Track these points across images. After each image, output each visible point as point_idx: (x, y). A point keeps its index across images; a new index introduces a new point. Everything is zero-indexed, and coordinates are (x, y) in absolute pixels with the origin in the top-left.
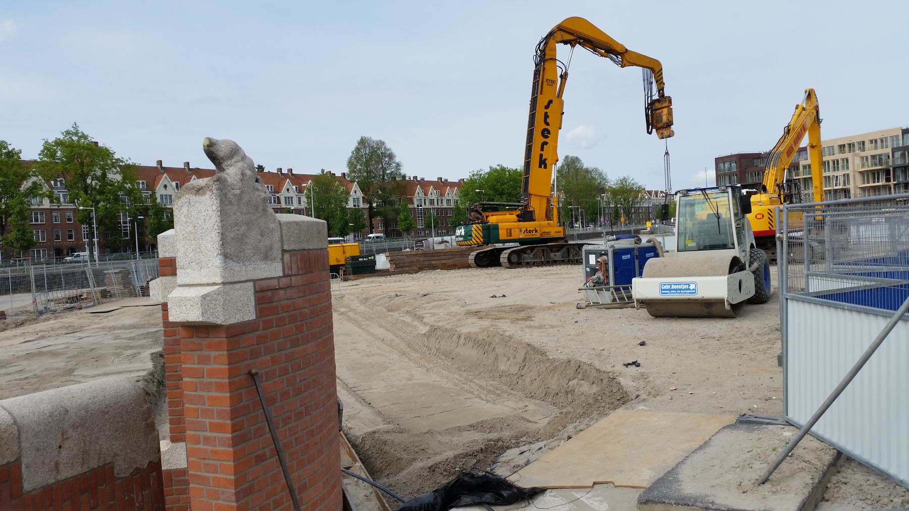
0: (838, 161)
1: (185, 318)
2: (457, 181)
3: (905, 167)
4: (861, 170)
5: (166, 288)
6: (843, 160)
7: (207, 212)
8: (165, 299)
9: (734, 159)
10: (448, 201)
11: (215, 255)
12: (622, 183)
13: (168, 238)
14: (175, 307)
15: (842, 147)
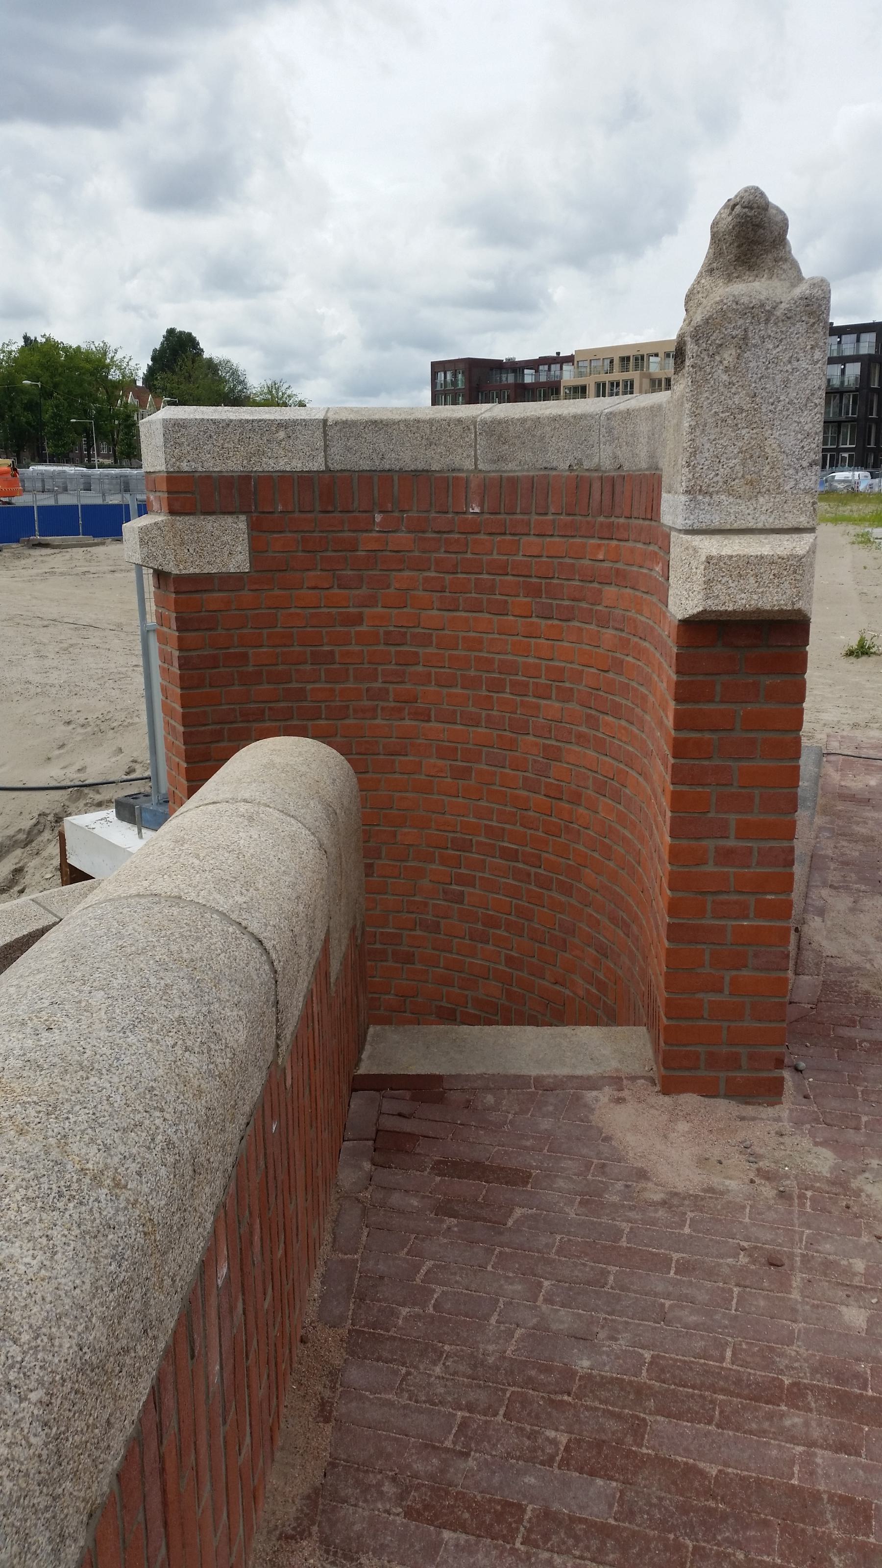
0: (604, 385)
1: (753, 602)
5: (182, 543)
7: (795, 364)
8: (181, 567)
11: (805, 464)
12: (270, 392)
13: (185, 427)
14: (725, 579)
15: (625, 360)
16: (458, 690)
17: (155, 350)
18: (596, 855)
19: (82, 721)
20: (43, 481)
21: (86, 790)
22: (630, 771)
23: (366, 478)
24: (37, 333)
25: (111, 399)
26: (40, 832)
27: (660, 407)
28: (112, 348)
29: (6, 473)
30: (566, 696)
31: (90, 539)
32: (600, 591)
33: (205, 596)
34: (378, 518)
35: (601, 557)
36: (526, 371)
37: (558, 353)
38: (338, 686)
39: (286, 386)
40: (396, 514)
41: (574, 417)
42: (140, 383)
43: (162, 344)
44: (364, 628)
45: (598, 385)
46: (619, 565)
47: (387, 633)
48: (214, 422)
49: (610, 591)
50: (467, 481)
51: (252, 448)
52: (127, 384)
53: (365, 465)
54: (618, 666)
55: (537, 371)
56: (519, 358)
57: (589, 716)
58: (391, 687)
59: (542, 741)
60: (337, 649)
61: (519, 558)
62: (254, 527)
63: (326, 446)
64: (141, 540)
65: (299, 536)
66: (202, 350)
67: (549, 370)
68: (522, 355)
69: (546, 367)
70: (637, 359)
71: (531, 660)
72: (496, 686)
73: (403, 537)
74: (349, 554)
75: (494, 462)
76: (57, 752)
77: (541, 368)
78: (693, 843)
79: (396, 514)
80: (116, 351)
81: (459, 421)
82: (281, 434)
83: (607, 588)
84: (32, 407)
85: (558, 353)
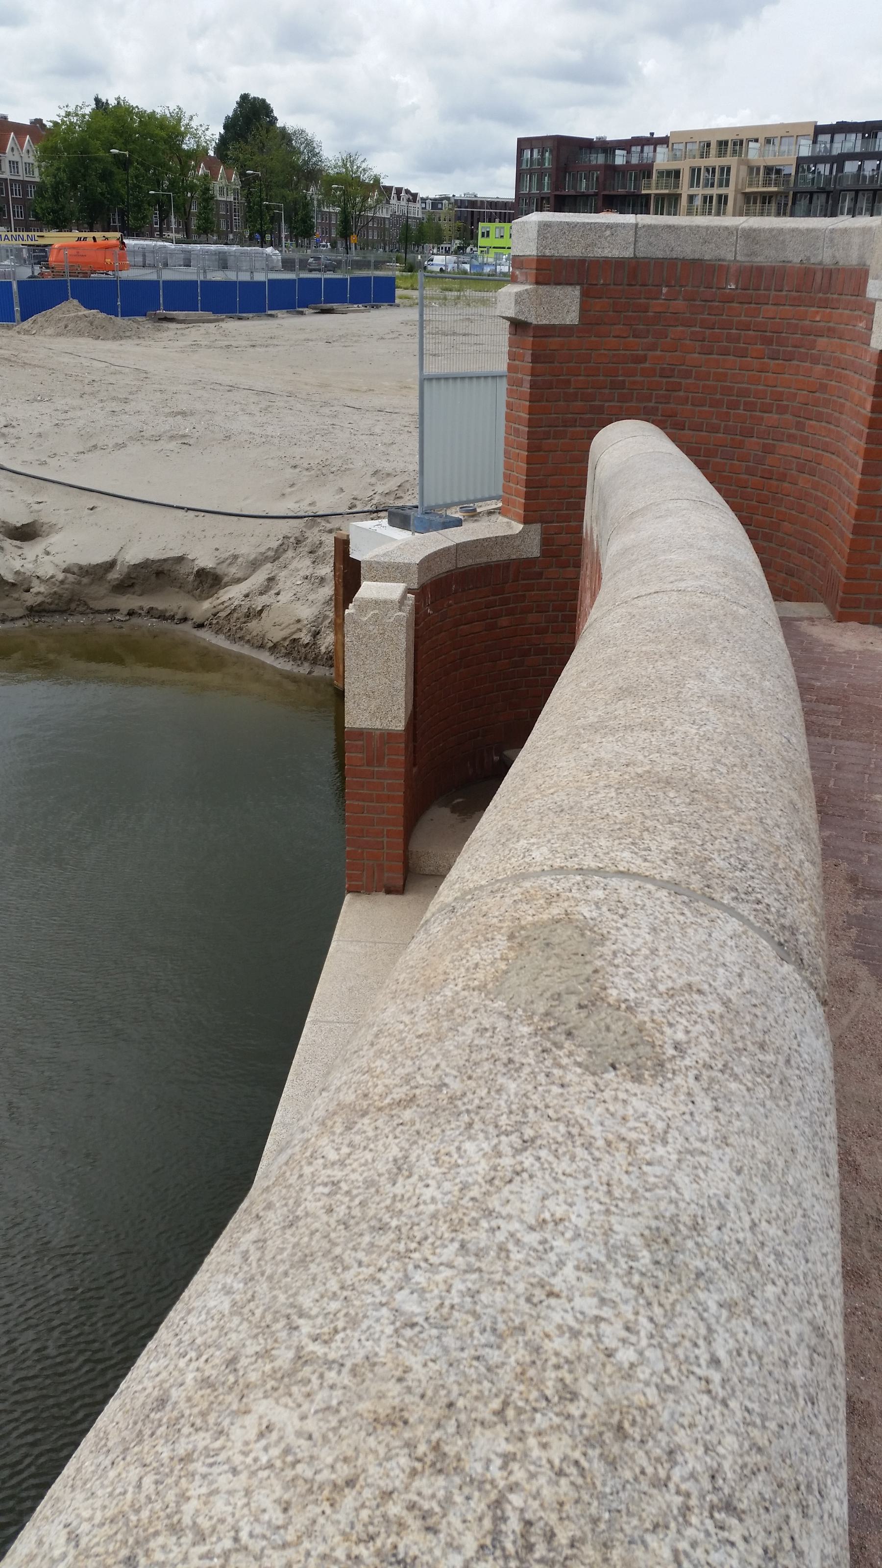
0: (699, 170)
2: (28, 123)
3: (875, 191)
4: (748, 190)
6: (722, 169)
9: (549, 144)
10: (13, 164)
12: (345, 165)
16: (706, 408)
17: (227, 118)
18: (794, 512)
19: (306, 465)
20: (144, 256)
21: (319, 520)
22: (825, 454)
23: (659, 263)
24: (110, 97)
25: (184, 169)
26: (285, 551)
27: (870, 229)
28: (187, 115)
29: (115, 246)
30: (782, 410)
31: (209, 315)
32: (815, 341)
33: (551, 339)
34: (664, 290)
35: (818, 319)
36: (617, 152)
37: (652, 134)
38: (625, 405)
39: (361, 159)
40: (677, 288)
41: (807, 230)
42: (211, 153)
43: (235, 111)
44: (647, 365)
45: (693, 170)
46: (831, 324)
47: (662, 369)
48: (568, 223)
49: (822, 341)
50: (728, 267)
51: (589, 241)
52: (199, 154)
53: (660, 254)
54: (824, 388)
55: (629, 152)
56: (610, 137)
57: (798, 423)
58: (660, 406)
59: (762, 441)
60: (627, 379)
61: (760, 319)
62: (584, 294)
63: (636, 241)
64: (516, 301)
65: (611, 301)
66: (276, 119)
67: (642, 151)
68: (614, 133)
69: (639, 148)
70: (735, 144)
71: (760, 387)
72: (734, 405)
73: (680, 304)
74: (642, 314)
75: (748, 255)
76: (289, 490)
77: (633, 149)
78: (873, 478)
79: (677, 288)
80: (191, 118)
81: (727, 228)
82: (608, 233)
83: (820, 339)
84: (106, 176)
85: (652, 134)
